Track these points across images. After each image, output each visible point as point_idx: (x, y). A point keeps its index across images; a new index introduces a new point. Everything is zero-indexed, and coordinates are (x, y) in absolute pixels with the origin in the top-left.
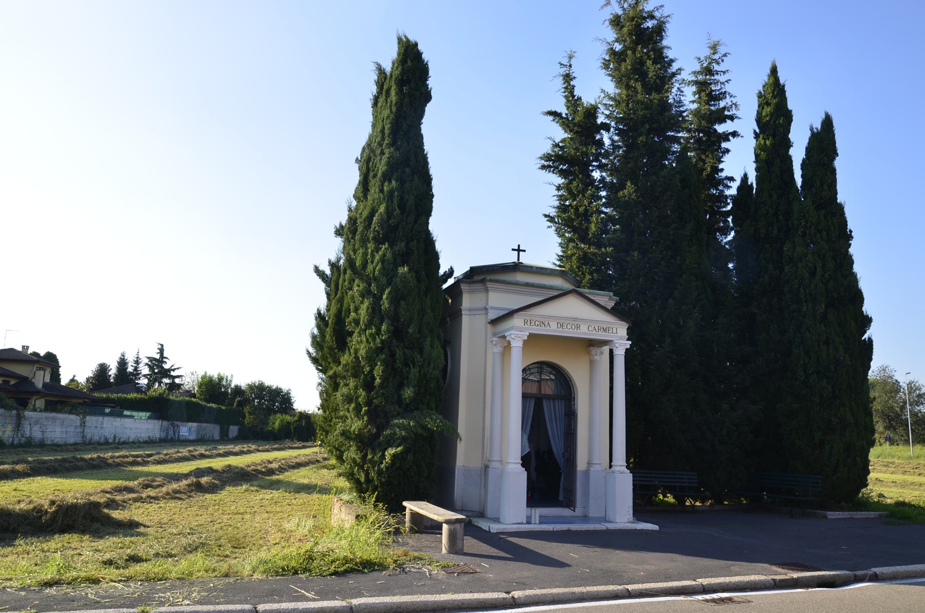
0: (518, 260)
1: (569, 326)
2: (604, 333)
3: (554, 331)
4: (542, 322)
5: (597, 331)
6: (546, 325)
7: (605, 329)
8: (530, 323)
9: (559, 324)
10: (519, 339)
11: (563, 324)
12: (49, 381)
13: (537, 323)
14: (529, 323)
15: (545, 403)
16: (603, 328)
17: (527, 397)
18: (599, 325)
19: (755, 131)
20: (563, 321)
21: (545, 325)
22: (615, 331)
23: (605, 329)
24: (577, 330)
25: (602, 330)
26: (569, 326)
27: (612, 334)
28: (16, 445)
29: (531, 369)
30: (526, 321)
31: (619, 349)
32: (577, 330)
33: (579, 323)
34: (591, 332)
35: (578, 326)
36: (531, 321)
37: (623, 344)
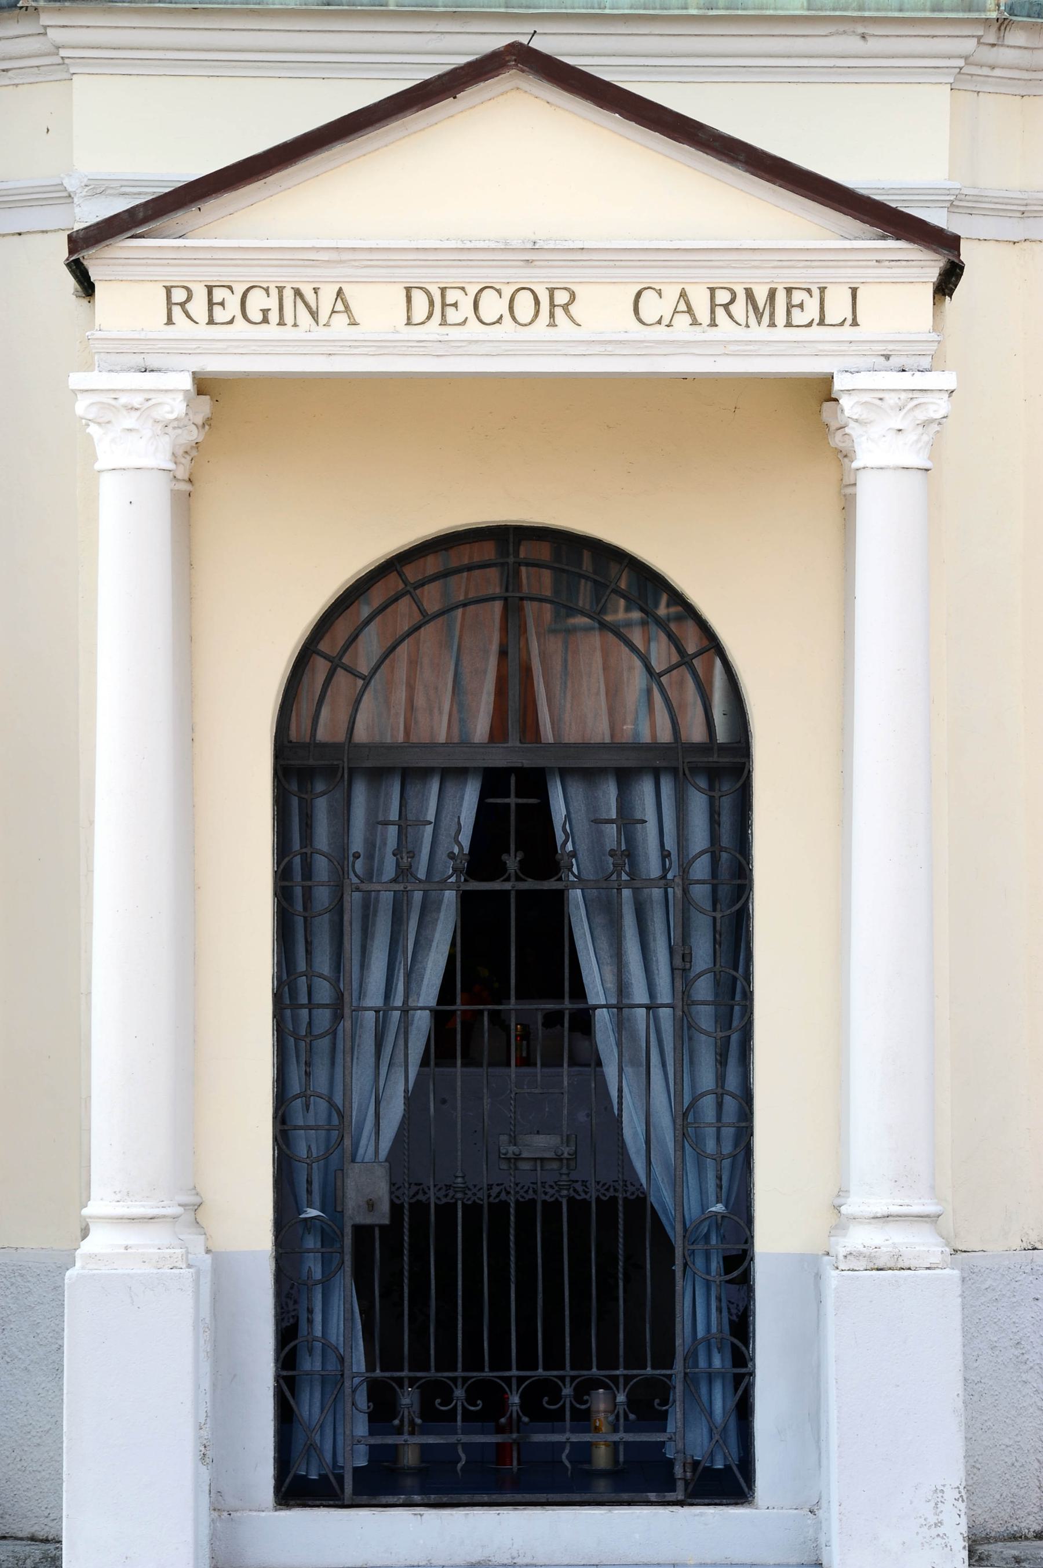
0: (528, 43)
1: (493, 306)
2: (760, 332)
3: (381, 347)
4: (298, 293)
5: (703, 313)
6: (324, 315)
7: (761, 297)
8: (211, 304)
10: (130, 421)
11: (451, 297)
13: (257, 302)
14: (198, 307)
15: (523, 569)
16: (750, 295)
17: (425, 773)
19: (803, 3)
20: (450, 276)
21: (314, 315)
22: (838, 307)
23: (761, 297)
24: (552, 324)
25: (739, 308)
26: (493, 306)
30: (179, 296)
32: (552, 324)
33: (559, 276)
35: (562, 298)
36: (218, 295)
37: (891, 399)
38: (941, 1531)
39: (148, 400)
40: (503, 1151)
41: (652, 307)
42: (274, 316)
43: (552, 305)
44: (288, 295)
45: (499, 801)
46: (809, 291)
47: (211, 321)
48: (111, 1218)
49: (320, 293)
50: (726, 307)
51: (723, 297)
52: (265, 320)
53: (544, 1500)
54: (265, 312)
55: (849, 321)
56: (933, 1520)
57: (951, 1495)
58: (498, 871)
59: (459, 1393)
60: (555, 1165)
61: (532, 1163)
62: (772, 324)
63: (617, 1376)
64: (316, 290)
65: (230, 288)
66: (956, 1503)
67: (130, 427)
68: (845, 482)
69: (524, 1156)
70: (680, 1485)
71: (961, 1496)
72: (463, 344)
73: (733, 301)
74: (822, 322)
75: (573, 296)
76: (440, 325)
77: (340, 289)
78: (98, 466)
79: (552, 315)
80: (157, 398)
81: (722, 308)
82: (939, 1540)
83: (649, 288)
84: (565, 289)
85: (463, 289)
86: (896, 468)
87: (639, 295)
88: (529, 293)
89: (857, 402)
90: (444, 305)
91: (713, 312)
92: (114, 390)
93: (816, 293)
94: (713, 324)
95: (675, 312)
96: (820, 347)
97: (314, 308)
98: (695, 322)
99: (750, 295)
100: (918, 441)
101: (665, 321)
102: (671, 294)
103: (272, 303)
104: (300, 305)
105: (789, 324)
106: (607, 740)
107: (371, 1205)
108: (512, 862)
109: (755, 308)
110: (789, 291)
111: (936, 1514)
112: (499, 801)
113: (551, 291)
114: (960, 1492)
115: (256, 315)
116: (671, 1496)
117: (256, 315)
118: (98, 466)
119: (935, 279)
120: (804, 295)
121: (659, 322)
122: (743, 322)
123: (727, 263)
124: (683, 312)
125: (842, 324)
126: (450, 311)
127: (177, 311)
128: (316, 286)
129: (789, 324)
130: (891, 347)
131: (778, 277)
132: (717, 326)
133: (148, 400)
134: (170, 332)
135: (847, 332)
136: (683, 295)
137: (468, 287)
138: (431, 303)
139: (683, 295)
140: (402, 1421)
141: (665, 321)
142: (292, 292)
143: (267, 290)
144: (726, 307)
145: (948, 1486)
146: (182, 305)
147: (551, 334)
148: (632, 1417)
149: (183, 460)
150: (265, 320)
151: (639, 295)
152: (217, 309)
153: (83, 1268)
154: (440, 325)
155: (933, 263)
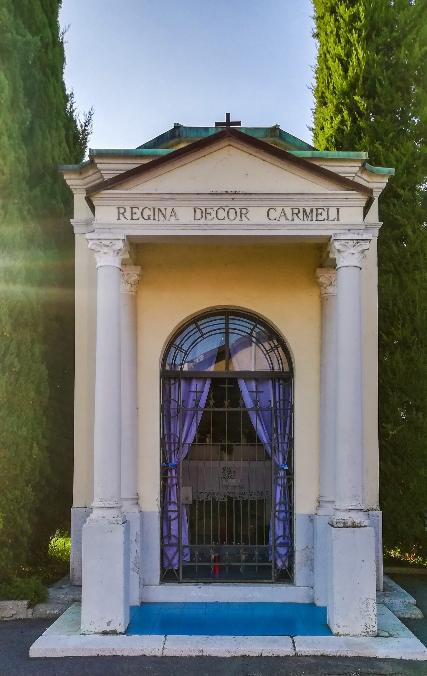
2: (307, 222)
3: (186, 226)
4: (160, 210)
7: (308, 210)
8: (132, 213)
9: (198, 211)
10: (106, 250)
12: (166, 369)
13: (147, 213)
14: (128, 214)
15: (242, 384)
16: (304, 211)
18: (294, 204)
21: (165, 216)
22: (333, 213)
25: (301, 215)
27: (326, 222)
28: (268, 379)
29: (274, 352)
31: (344, 254)
34: (276, 222)
35: (244, 211)
36: (134, 210)
38: (368, 613)
39: (111, 243)
40: (224, 484)
41: (273, 215)
42: (152, 217)
43: (241, 213)
44: (157, 210)
45: (223, 386)
46: (324, 209)
47: (132, 219)
48: (98, 507)
49: (166, 209)
50: (297, 214)
51: (296, 211)
52: (149, 218)
53: (235, 582)
54: (149, 216)
55: (337, 219)
56: (365, 610)
57: (371, 602)
58: (222, 406)
59: (212, 551)
60: (238, 488)
61: (232, 487)
62: (312, 220)
63: (256, 547)
64: (165, 209)
65: (138, 208)
66: (373, 604)
67: (105, 252)
68: (321, 294)
69: (230, 485)
70: (273, 578)
71: (375, 602)
72: (213, 225)
73: (299, 212)
74: (328, 219)
75: (248, 211)
76: (205, 220)
77: (173, 208)
78: (97, 266)
79: (241, 217)
80: (115, 242)
81: (295, 215)
82: (367, 617)
83: (271, 208)
84: (245, 208)
85: (212, 208)
86: (352, 266)
87: (269, 210)
88: (233, 210)
89: (340, 244)
90: (206, 213)
91: (293, 216)
92: (100, 239)
93: (326, 210)
94: (293, 220)
95: (280, 216)
96: (328, 227)
97: (165, 214)
98: (287, 220)
99: (304, 211)
100: (358, 258)
101: (277, 219)
102: (279, 210)
103: (151, 213)
104: (160, 213)
105: (317, 220)
106: (159, 654)
107: (187, 498)
108: (227, 403)
109: (306, 214)
110: (317, 209)
111: (366, 608)
112: (223, 386)
113: (241, 209)
114: (374, 601)
115: (146, 217)
116: (270, 581)
117: (146, 217)
118: (97, 266)
119: (364, 206)
120: (322, 211)
121: (275, 219)
122: (302, 219)
123: (297, 199)
124: (283, 216)
125: (334, 220)
126: (208, 216)
127: (121, 216)
128: (166, 207)
129: (317, 220)
130: (351, 227)
131: (314, 204)
132: (294, 220)
133: (111, 243)
134: (119, 222)
135: (336, 222)
136: (283, 210)
137: (214, 208)
138: (202, 213)
139: (283, 210)
140: (196, 559)
141: (277, 219)
142: (158, 210)
143: (150, 209)
144: (297, 214)
145: (370, 599)
146: (123, 213)
147: (240, 222)
148: (260, 558)
149: (134, 286)
150: (149, 218)
151: (269, 210)
152: (134, 215)
153: (89, 524)
154: (205, 220)
155: (364, 199)
